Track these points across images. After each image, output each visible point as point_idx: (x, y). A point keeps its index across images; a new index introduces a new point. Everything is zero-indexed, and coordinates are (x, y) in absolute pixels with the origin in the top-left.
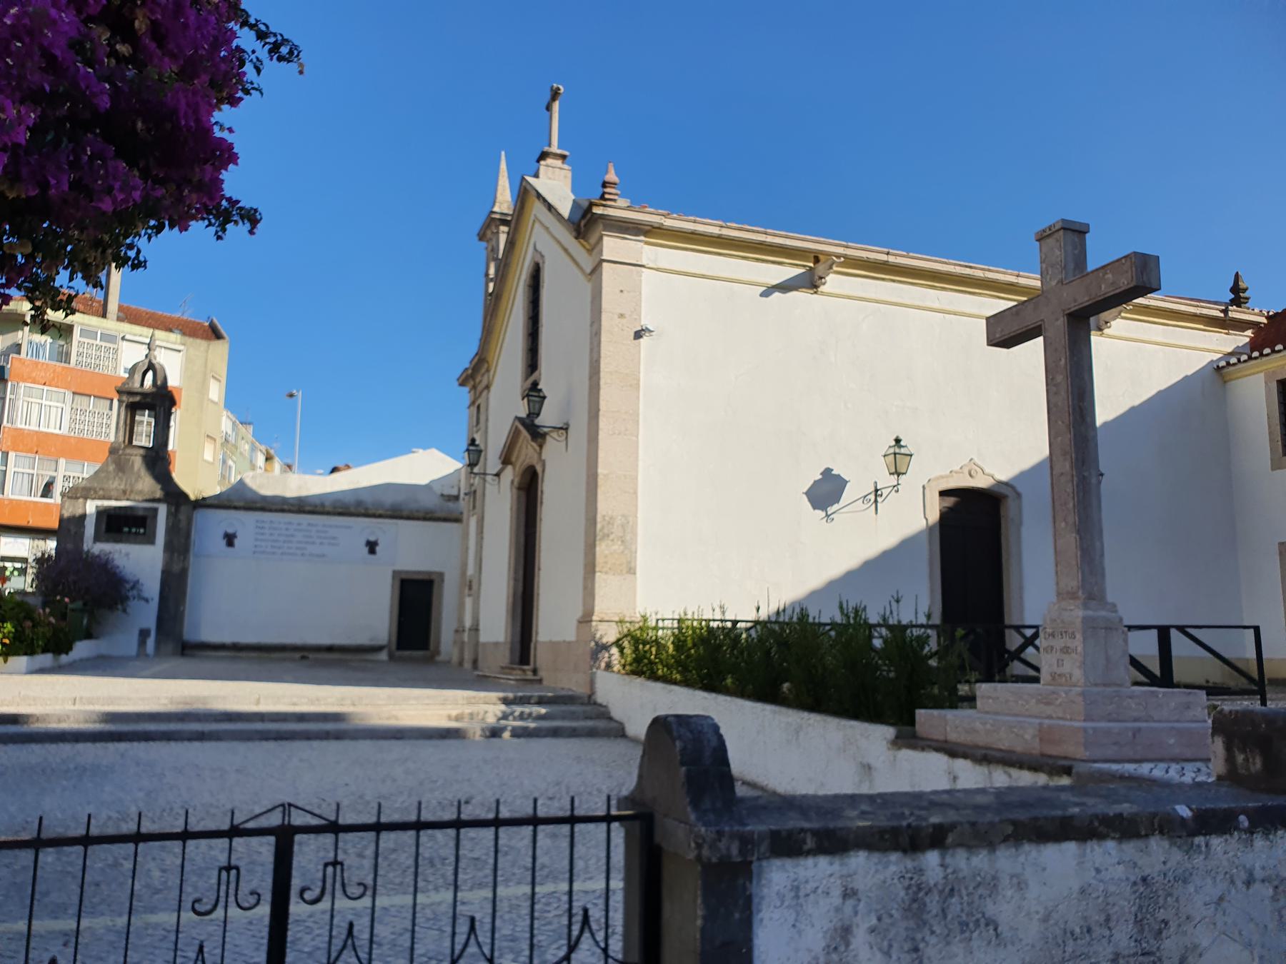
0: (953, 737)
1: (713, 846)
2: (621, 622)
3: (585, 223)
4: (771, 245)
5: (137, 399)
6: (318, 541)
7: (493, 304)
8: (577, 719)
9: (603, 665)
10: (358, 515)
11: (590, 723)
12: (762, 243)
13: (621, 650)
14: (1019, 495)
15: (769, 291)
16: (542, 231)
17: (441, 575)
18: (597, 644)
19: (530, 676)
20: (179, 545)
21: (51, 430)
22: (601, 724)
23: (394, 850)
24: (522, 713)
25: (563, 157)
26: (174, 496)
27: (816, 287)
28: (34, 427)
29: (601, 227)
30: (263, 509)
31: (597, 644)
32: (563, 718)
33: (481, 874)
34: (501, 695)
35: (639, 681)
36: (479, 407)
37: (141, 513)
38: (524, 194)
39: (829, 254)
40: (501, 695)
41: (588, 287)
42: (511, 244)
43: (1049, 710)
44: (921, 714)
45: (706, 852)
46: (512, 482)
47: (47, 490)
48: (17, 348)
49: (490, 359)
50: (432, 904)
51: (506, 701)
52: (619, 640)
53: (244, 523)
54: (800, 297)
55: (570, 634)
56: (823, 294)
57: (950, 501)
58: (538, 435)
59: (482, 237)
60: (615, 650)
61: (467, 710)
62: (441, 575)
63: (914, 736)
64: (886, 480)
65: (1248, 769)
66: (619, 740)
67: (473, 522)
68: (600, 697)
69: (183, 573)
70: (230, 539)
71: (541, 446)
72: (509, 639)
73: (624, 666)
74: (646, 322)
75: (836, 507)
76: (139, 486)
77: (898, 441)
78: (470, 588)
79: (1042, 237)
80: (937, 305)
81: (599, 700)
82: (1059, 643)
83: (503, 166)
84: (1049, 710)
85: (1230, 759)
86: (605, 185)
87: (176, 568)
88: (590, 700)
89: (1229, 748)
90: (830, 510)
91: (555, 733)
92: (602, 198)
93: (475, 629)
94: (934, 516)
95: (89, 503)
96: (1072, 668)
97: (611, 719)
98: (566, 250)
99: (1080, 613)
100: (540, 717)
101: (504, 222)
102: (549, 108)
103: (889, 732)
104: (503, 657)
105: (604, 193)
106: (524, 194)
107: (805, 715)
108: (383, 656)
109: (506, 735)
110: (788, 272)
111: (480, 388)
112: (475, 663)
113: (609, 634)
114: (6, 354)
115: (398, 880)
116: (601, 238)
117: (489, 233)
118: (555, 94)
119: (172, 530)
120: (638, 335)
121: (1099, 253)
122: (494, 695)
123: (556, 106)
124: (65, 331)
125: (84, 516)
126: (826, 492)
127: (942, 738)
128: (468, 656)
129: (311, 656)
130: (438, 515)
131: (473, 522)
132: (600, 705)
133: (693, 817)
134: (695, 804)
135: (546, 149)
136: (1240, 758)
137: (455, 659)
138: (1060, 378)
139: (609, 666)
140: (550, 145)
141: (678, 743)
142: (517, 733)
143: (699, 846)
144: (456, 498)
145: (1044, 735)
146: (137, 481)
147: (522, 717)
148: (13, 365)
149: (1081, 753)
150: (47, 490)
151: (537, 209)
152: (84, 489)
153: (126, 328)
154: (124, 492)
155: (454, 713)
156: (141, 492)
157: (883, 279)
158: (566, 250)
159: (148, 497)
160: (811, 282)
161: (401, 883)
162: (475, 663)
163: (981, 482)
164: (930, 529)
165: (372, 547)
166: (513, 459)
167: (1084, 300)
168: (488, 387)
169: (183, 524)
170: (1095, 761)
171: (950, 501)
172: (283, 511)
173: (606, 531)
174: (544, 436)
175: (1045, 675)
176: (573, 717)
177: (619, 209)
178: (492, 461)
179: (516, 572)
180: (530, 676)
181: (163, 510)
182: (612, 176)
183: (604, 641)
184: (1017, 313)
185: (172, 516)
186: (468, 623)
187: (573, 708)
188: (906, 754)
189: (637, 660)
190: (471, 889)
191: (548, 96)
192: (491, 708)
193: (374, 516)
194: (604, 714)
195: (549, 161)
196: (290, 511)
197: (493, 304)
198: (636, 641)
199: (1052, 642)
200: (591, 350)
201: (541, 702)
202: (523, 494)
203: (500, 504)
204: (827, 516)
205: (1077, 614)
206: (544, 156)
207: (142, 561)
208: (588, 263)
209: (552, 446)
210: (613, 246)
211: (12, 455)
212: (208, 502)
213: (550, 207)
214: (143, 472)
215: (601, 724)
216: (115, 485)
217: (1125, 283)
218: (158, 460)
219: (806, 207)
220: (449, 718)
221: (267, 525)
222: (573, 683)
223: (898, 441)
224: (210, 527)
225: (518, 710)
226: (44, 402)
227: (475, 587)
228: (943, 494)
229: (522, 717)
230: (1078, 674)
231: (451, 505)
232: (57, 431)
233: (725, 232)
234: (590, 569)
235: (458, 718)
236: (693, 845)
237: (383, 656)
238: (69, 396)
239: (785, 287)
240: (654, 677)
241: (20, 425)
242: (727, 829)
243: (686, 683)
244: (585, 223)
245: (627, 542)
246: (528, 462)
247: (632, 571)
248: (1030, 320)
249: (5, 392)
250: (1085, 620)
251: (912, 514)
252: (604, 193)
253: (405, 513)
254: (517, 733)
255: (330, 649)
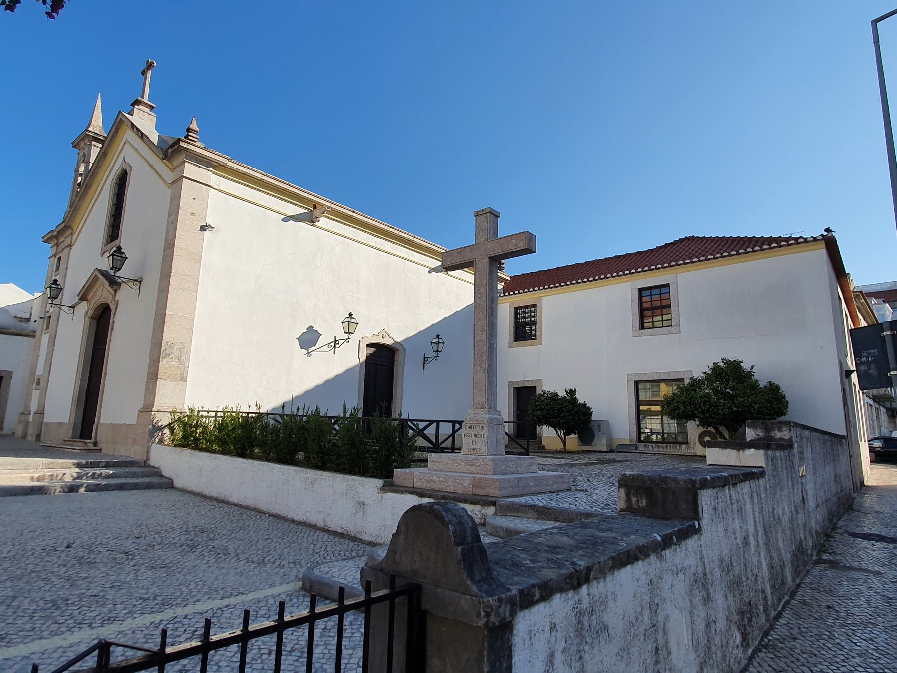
0: (418, 484)
1: (498, 614)
2: (174, 412)
3: (171, 151)
4: (291, 192)
7: (82, 191)
8: (137, 477)
9: (157, 440)
11: (147, 480)
12: (286, 190)
13: (172, 430)
14: (405, 350)
15: (287, 219)
16: (132, 150)
17: (10, 374)
18: (154, 426)
19: (91, 446)
22: (156, 480)
23: (15, 598)
24: (94, 474)
25: (152, 108)
27: (314, 222)
29: (184, 156)
31: (154, 426)
32: (126, 477)
33: (105, 610)
34: (75, 461)
35: (188, 452)
36: (59, 259)
38: (118, 124)
39: (322, 205)
40: (75, 461)
41: (168, 193)
42: (103, 155)
43: (472, 469)
44: (397, 471)
45: (493, 618)
46: (86, 313)
50: (71, 646)
51: (79, 465)
52: (170, 424)
55: (131, 418)
56: (317, 227)
57: (372, 350)
58: (114, 283)
59: (75, 145)
60: (167, 431)
61: (48, 473)
62: (10, 374)
63: (392, 484)
64: (342, 335)
65: (638, 505)
66: (169, 490)
67: (45, 338)
68: (153, 462)
71: (116, 291)
72: (72, 421)
73: (173, 441)
74: (209, 221)
75: (314, 348)
77: (351, 315)
78: (38, 384)
79: (478, 215)
80: (374, 245)
81: (152, 464)
82: (474, 432)
83: (99, 103)
84: (472, 469)
85: (628, 500)
86: (189, 130)
88: (145, 464)
89: (628, 494)
91: (121, 487)
92: (187, 137)
93: (41, 413)
94: (363, 359)
96: (481, 445)
97: (163, 476)
98: (151, 166)
99: (487, 416)
100: (108, 476)
101: (97, 140)
102: (143, 73)
103: (379, 482)
104: (67, 433)
105: (188, 135)
106: (118, 124)
107: (320, 472)
109: (82, 490)
110: (300, 211)
111: (61, 246)
112: (38, 437)
113: (165, 420)
115: (28, 626)
116: (184, 162)
117: (82, 144)
118: (150, 66)
120: (203, 228)
121: (505, 229)
122: (69, 462)
123: (149, 73)
126: (309, 340)
127: (411, 485)
128: (32, 431)
130: (12, 330)
131: (45, 338)
132: (154, 467)
133: (475, 589)
134: (471, 576)
135: (139, 98)
136: (634, 499)
137: (19, 432)
138: (483, 290)
139: (161, 441)
140: (142, 97)
141: (450, 527)
142: (89, 489)
143: (488, 615)
144: (28, 320)
145: (476, 483)
147: (93, 476)
149: (497, 493)
151: (129, 135)
155: (36, 475)
158: (151, 166)
160: (311, 219)
161: (34, 629)
162: (38, 437)
163: (388, 342)
164: (361, 364)
166: (89, 297)
167: (499, 251)
168: (70, 246)
170: (508, 497)
171: (372, 350)
173: (168, 352)
174: (119, 284)
175: (465, 449)
176: (134, 475)
177: (197, 148)
178: (69, 295)
179: (83, 375)
180: (91, 446)
182: (194, 126)
183: (160, 424)
184: (460, 252)
186: (34, 408)
187: (133, 469)
188: (389, 495)
189: (185, 437)
190: (102, 625)
191: (144, 66)
192: (67, 471)
194: (157, 473)
195: (141, 107)
197: (82, 191)
198: (185, 425)
199: (470, 431)
200: (167, 232)
201: (107, 465)
202: (95, 323)
203: (73, 330)
204: (309, 353)
205: (485, 416)
206: (137, 102)
208: (170, 177)
209: (125, 294)
210: (190, 169)
213: (142, 135)
215: (156, 480)
217: (522, 246)
219: (325, 175)
220: (32, 479)
222: (134, 453)
223: (351, 315)
225: (91, 471)
227: (42, 383)
228: (368, 346)
229: (93, 476)
230: (484, 449)
231: (22, 324)
233: (265, 178)
234: (153, 376)
235: (38, 479)
236: (483, 614)
239: (296, 218)
240: (197, 448)
242: (504, 596)
243: (223, 452)
244: (171, 151)
245: (182, 360)
246: (102, 300)
247: (184, 379)
248: (468, 257)
250: (490, 420)
251: (351, 357)
252: (188, 135)
254: (89, 489)
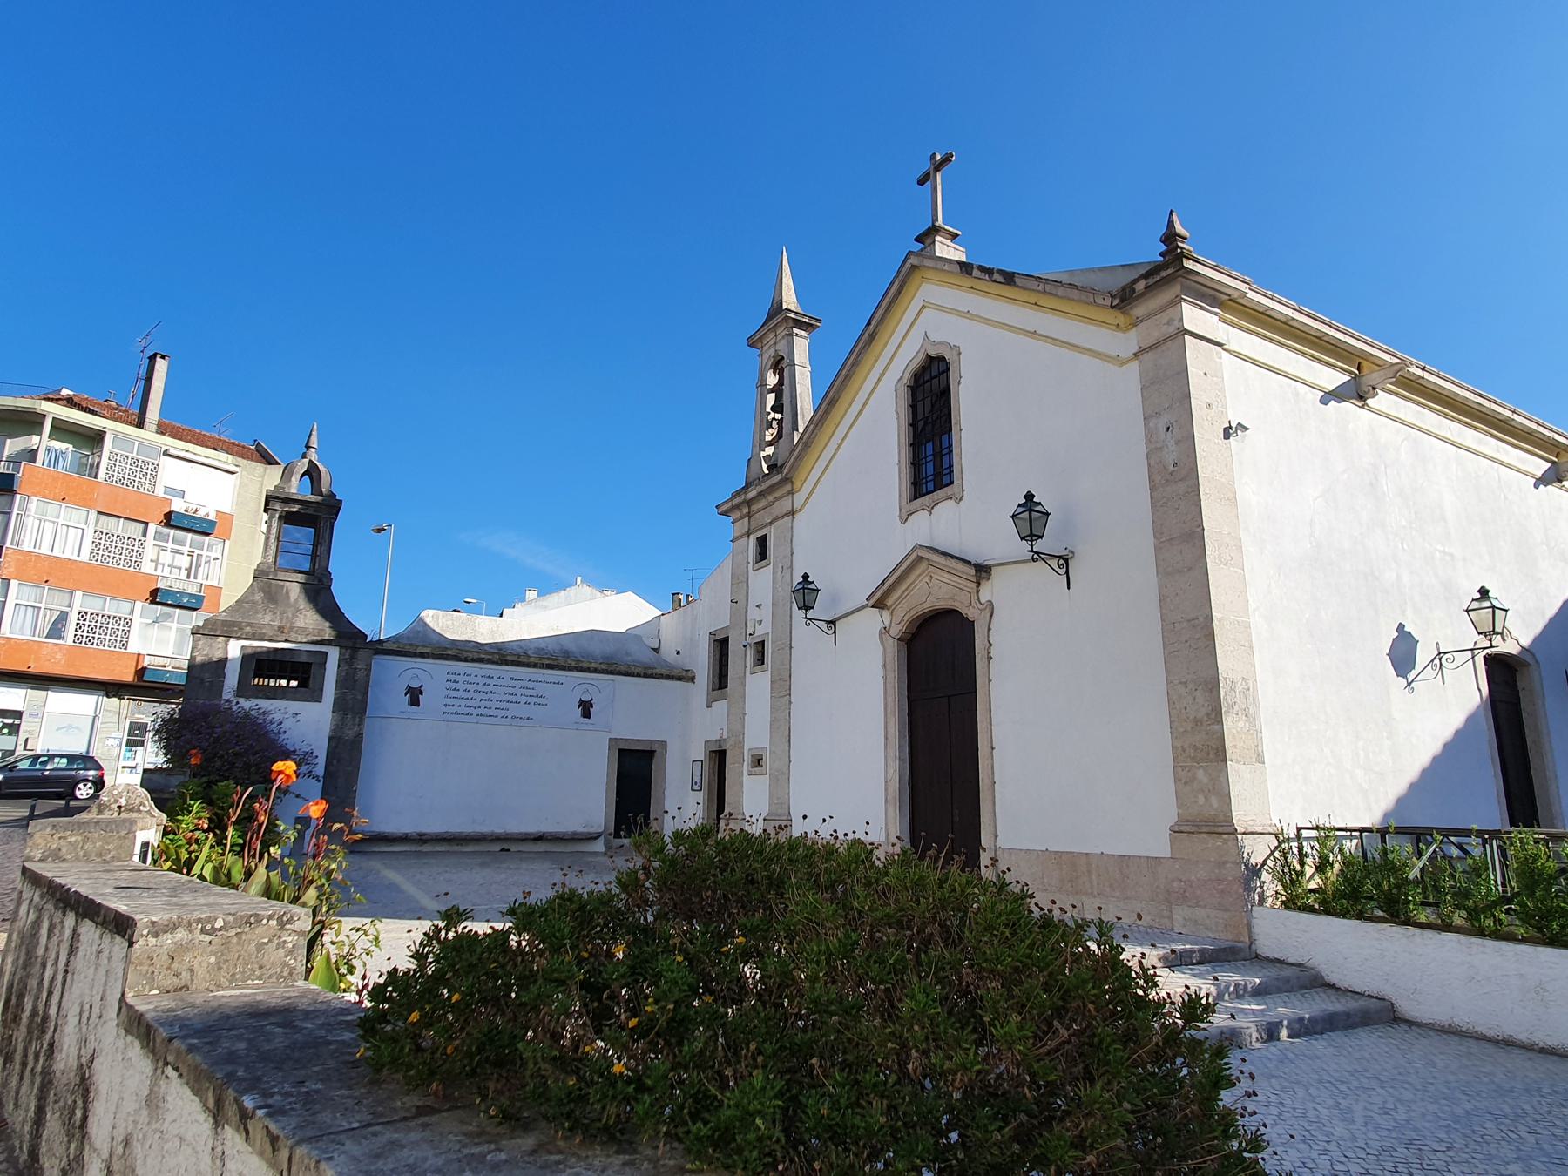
5: (296, 508)
6: (523, 699)
10: (570, 669)
20: (353, 703)
21: (67, 555)
25: (954, 237)
26: (349, 637)
28: (45, 550)
30: (456, 658)
37: (304, 659)
47: (56, 631)
48: (32, 454)
49: (797, 484)
53: (430, 675)
54: (1349, 408)
69: (358, 740)
70: (414, 696)
76: (300, 622)
87: (349, 733)
90: (1411, 676)
95: (232, 642)
108: (599, 846)
109: (1284, 1034)
114: (15, 460)
119: (344, 683)
120: (1227, 433)
124: (94, 439)
125: (223, 662)
129: (514, 848)
146: (294, 616)
148: (24, 473)
150: (56, 631)
152: (225, 623)
153: (168, 442)
154: (281, 629)
156: (302, 630)
157: (1410, 400)
159: (310, 638)
165: (586, 708)
169: (360, 675)
172: (481, 661)
181: (334, 654)
183: (1252, 861)
185: (346, 662)
193: (588, 670)
196: (490, 661)
207: (307, 722)
211: (14, 584)
212: (387, 646)
214: (303, 603)
216: (266, 619)
218: (319, 590)
221: (461, 679)
224: (393, 675)
226: (61, 521)
232: (75, 557)
237: (599, 846)
238: (93, 514)
241: (27, 546)
249: (11, 507)
253: (622, 668)
254: (1302, 1029)
255: (540, 838)
